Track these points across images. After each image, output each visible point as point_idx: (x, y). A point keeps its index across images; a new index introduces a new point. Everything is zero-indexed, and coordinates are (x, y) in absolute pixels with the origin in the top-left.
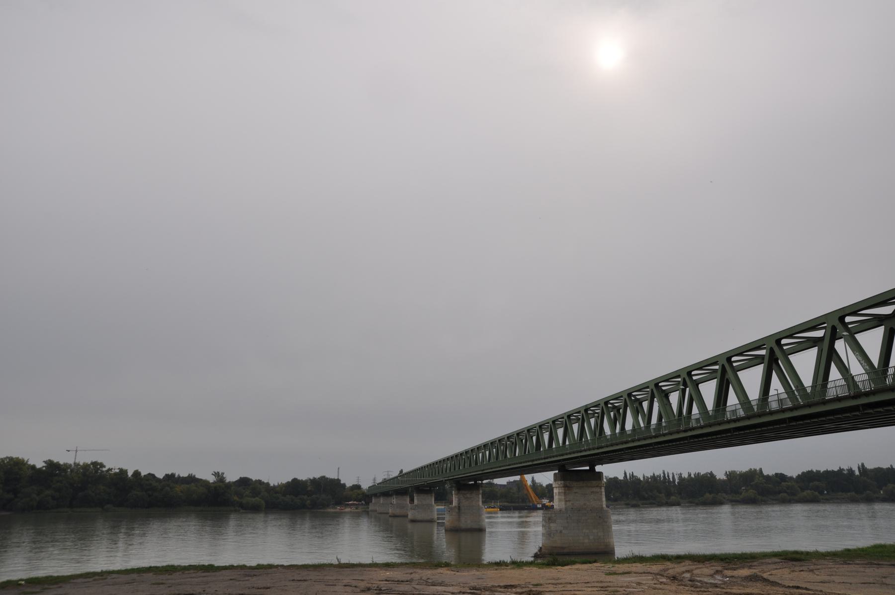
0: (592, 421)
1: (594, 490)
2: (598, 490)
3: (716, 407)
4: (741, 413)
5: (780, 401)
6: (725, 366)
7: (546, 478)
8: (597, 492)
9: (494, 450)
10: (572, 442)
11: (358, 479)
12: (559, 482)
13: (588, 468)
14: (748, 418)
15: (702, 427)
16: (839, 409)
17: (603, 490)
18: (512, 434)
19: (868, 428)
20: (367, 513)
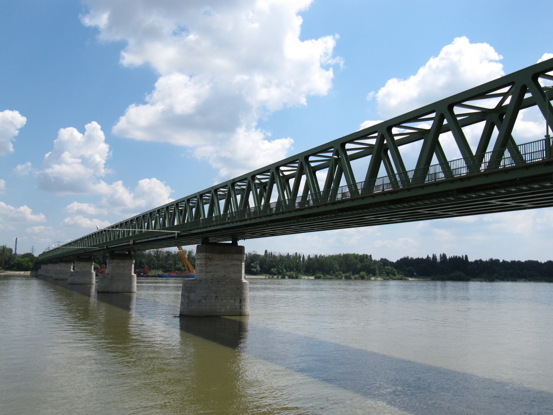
0: (239, 197)
1: (234, 262)
2: (238, 263)
3: (369, 179)
4: (442, 175)
5: (343, 194)
6: (274, 173)
7: (192, 248)
8: (238, 265)
9: (161, 219)
10: (216, 215)
11: (33, 248)
12: (202, 254)
13: (231, 242)
14: (351, 200)
15: (283, 213)
16: (320, 212)
17: (243, 264)
18: (133, 218)
19: (355, 227)
20: (37, 277)
